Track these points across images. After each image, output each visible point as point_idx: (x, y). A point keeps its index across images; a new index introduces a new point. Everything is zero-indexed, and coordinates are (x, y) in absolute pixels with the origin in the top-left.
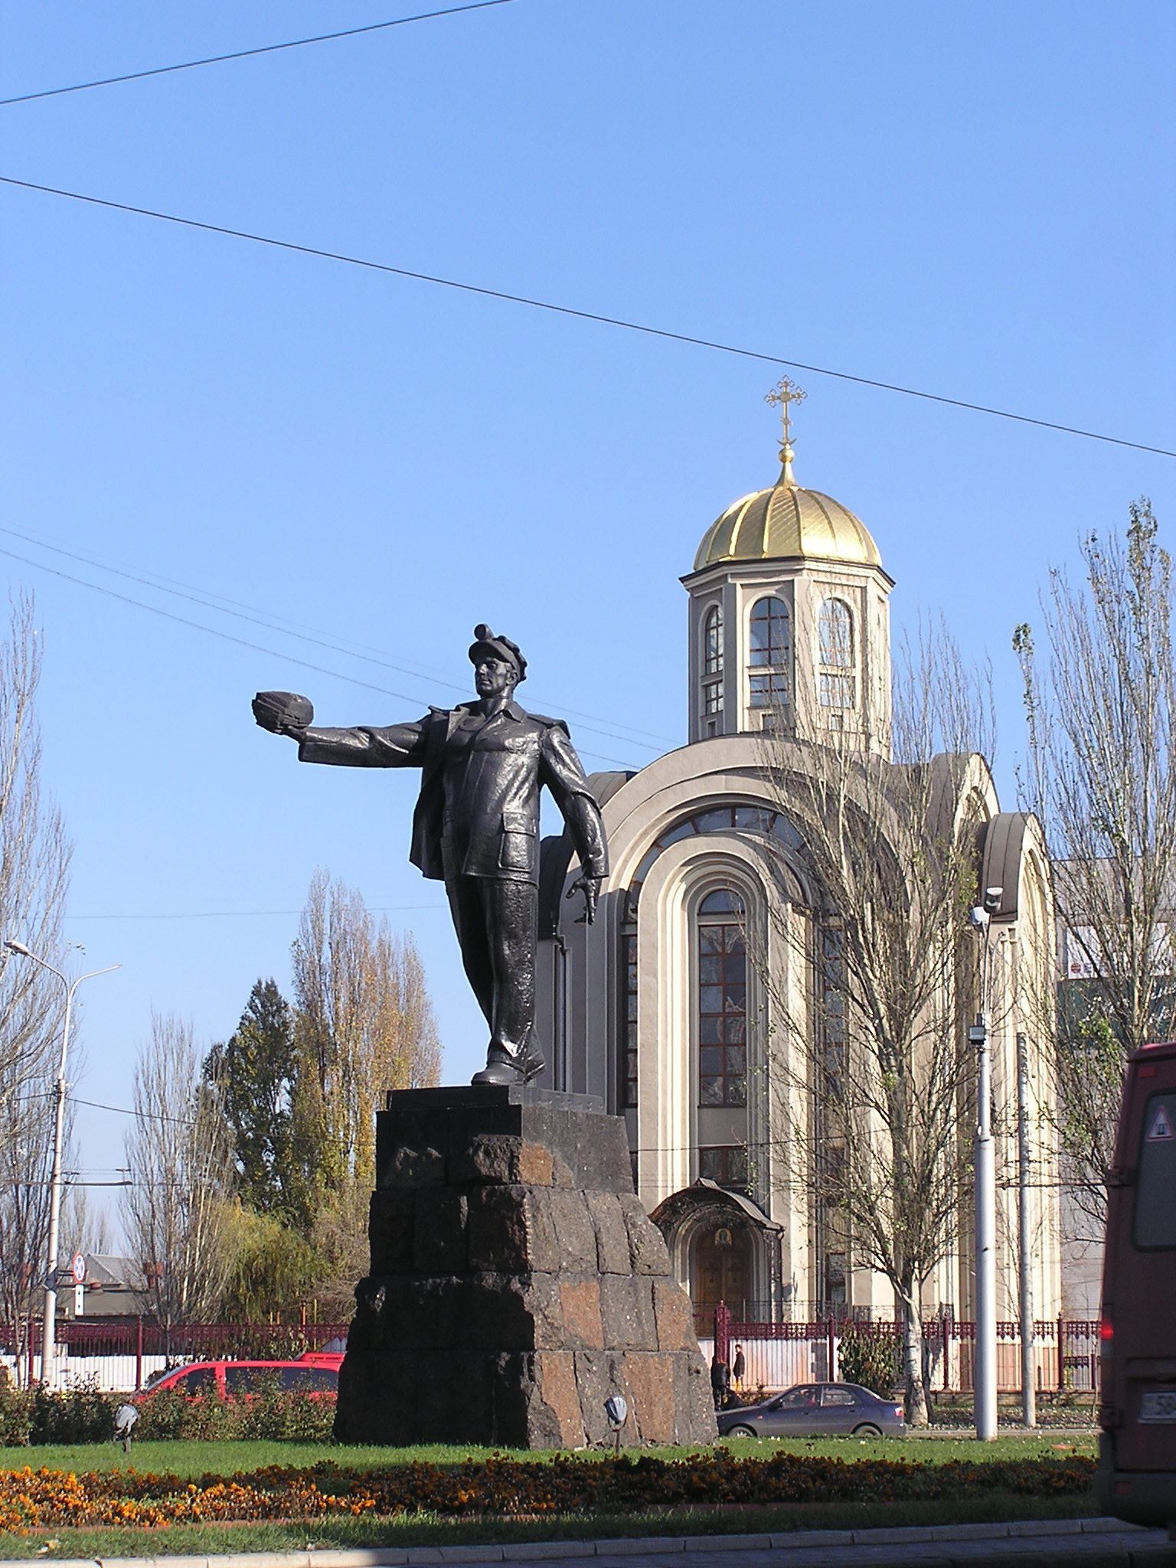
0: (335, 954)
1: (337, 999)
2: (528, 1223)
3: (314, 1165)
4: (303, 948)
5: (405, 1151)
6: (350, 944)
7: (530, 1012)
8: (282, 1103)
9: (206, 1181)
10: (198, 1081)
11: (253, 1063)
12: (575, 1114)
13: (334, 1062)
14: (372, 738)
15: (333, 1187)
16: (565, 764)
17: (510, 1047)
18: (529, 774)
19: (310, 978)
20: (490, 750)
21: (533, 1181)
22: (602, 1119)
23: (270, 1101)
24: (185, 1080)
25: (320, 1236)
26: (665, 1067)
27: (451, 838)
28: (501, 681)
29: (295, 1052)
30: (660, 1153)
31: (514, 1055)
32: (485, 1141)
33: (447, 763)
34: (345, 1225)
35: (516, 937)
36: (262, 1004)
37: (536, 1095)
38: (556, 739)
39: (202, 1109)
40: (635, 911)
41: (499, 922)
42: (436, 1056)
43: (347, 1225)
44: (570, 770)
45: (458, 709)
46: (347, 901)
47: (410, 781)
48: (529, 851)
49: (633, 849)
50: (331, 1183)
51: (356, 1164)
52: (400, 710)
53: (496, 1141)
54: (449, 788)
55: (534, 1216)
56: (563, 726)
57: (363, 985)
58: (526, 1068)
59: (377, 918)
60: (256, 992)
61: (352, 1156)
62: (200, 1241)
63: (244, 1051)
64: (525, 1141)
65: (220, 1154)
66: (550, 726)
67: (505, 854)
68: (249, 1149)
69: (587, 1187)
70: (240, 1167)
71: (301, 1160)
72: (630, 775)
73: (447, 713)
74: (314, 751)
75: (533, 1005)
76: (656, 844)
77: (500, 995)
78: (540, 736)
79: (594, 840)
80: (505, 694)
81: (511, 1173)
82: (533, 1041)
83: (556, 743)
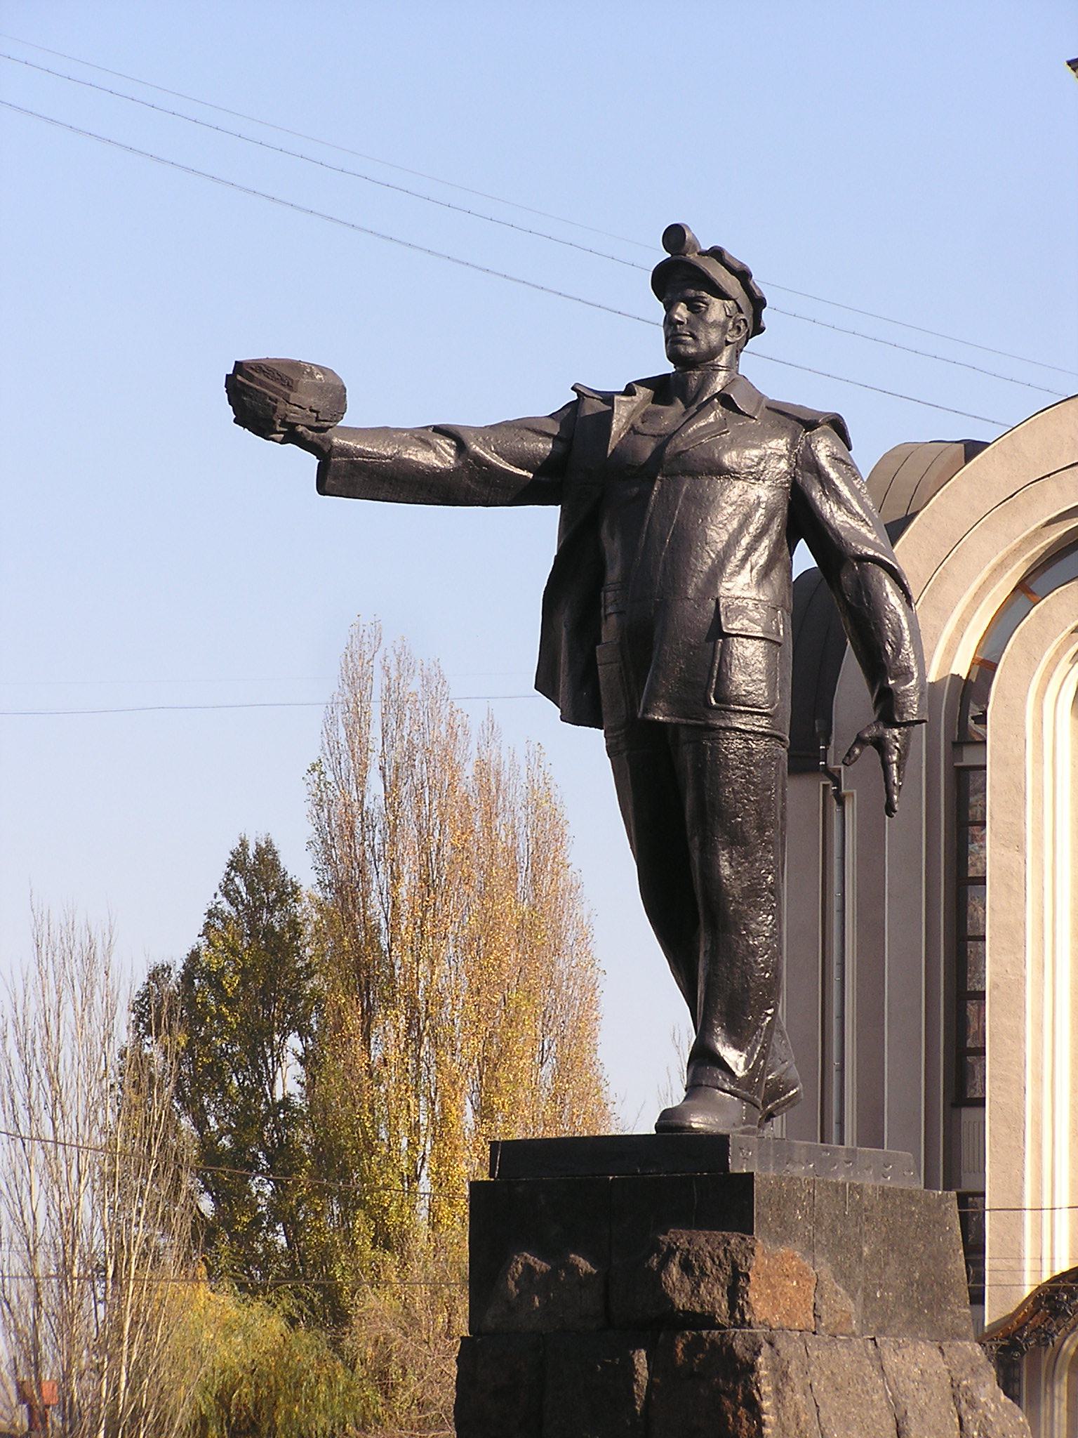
0: (391, 790)
1: (396, 877)
2: (766, 1404)
3: (351, 1203)
4: (330, 777)
5: (525, 1260)
6: (421, 771)
7: (772, 988)
8: (288, 1080)
9: (139, 1233)
10: (123, 1036)
11: (230, 1002)
12: (859, 1189)
13: (390, 1002)
14: (461, 447)
15: (387, 1246)
16: (840, 501)
17: (733, 1057)
18: (770, 518)
19: (342, 834)
20: (694, 474)
21: (776, 1321)
22: (911, 1197)
23: (265, 1078)
24: (98, 1039)
25: (361, 1341)
26: (1039, 1027)
27: (613, 642)
28: (714, 336)
29: (316, 981)
30: (1028, 1214)
31: (740, 1073)
32: (683, 1243)
33: (606, 491)
34: (410, 1322)
35: (744, 841)
36: (249, 887)
37: (782, 1151)
38: (824, 449)
39: (131, 1092)
40: (982, 719)
41: (711, 813)
42: (590, 989)
43: (415, 1323)
44: (850, 511)
45: (629, 391)
46: (415, 685)
47: (537, 531)
48: (770, 671)
49: (978, 597)
50: (384, 1240)
51: (437, 1227)
52: (513, 388)
53: (705, 1243)
54: (612, 546)
55: (778, 1391)
56: (837, 426)
57: (447, 851)
58: (763, 1097)
59: (475, 720)
60: (237, 864)
61: (425, 1185)
62: (130, 1353)
63: (215, 979)
64: (761, 1243)
65: (166, 1182)
66: (810, 425)
67: (723, 679)
68: (223, 1170)
69: (881, 1331)
70: (206, 1205)
71: (322, 1192)
72: (972, 449)
73: (608, 398)
74: (352, 474)
75: (777, 977)
76: (1023, 587)
77: (714, 957)
78: (793, 445)
79: (897, 650)
80: (723, 360)
81: (733, 1305)
82: (781, 1046)
83: (824, 461)
